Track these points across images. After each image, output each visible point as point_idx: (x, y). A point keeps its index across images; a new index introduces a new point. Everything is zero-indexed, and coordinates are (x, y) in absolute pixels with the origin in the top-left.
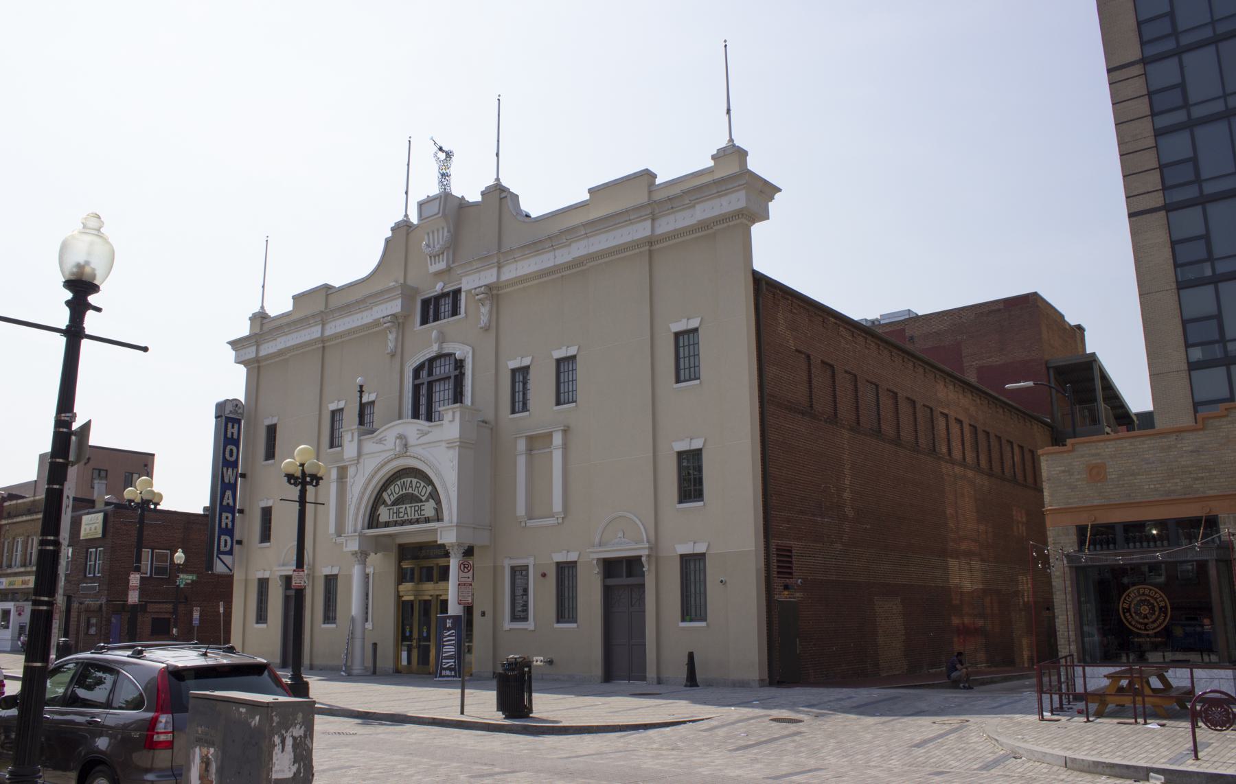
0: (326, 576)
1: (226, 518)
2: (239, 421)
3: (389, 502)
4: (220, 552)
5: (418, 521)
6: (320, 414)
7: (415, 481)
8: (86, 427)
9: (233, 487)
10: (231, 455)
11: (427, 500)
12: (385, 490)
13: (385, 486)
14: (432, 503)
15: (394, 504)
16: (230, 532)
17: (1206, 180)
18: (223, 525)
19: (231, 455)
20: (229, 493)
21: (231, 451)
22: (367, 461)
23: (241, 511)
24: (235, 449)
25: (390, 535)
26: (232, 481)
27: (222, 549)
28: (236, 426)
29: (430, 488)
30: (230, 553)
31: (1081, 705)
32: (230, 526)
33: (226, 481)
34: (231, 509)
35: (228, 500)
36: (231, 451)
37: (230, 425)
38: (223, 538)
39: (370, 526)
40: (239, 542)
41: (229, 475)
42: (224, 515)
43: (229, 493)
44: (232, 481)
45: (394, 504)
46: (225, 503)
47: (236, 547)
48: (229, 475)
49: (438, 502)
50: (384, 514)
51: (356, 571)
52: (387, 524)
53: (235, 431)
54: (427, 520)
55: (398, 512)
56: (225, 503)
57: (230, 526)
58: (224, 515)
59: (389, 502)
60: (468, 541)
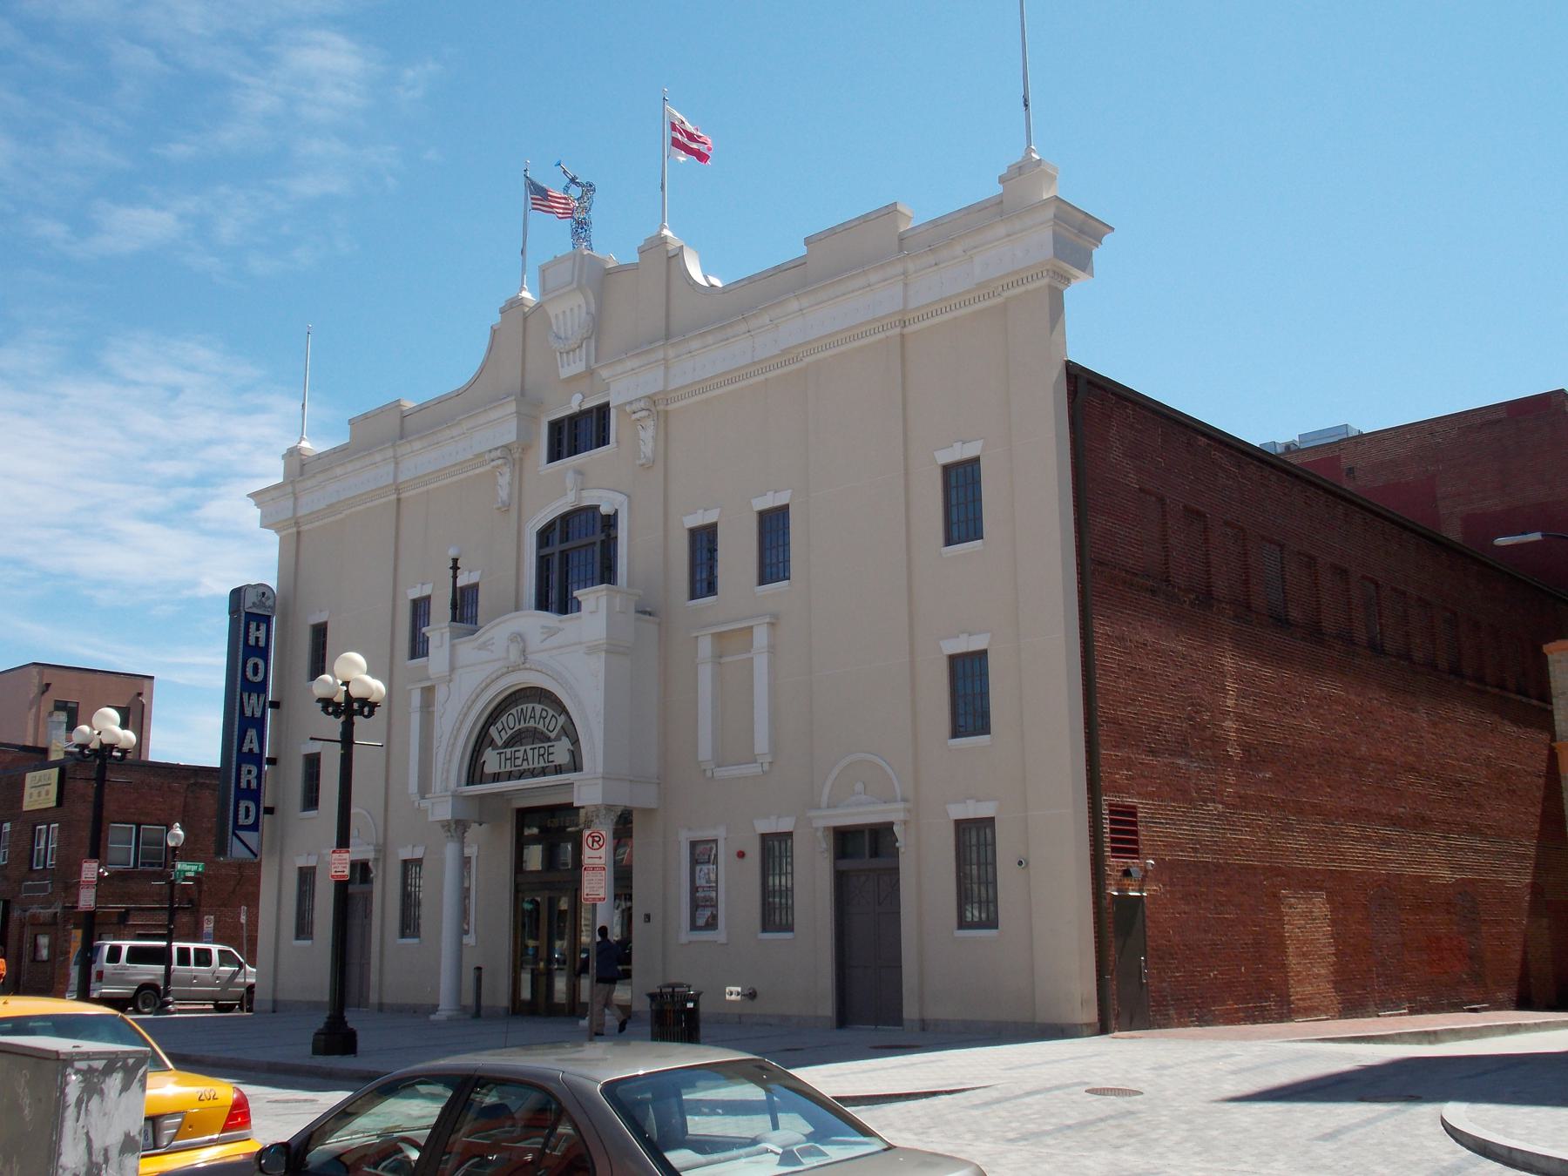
1: (248, 775)
3: (500, 743)
4: (237, 826)
7: (539, 707)
9: (259, 724)
10: (256, 672)
11: (558, 738)
15: (507, 744)
16: (254, 795)
18: (244, 785)
19: (256, 672)
20: (252, 733)
21: (256, 666)
22: (468, 672)
26: (258, 714)
27: (242, 821)
28: (263, 627)
29: (562, 719)
30: (255, 827)
32: (254, 785)
33: (248, 713)
34: (256, 759)
35: (251, 744)
36: (256, 666)
37: (253, 626)
38: (243, 804)
39: (471, 781)
40: (270, 811)
43: (252, 733)
44: (258, 714)
45: (507, 744)
46: (245, 749)
47: (266, 819)
48: (252, 705)
49: (575, 742)
50: (492, 761)
51: (450, 851)
52: (496, 777)
53: (262, 634)
54: (558, 770)
56: (245, 749)
57: (254, 785)
58: (245, 768)
60: (623, 800)
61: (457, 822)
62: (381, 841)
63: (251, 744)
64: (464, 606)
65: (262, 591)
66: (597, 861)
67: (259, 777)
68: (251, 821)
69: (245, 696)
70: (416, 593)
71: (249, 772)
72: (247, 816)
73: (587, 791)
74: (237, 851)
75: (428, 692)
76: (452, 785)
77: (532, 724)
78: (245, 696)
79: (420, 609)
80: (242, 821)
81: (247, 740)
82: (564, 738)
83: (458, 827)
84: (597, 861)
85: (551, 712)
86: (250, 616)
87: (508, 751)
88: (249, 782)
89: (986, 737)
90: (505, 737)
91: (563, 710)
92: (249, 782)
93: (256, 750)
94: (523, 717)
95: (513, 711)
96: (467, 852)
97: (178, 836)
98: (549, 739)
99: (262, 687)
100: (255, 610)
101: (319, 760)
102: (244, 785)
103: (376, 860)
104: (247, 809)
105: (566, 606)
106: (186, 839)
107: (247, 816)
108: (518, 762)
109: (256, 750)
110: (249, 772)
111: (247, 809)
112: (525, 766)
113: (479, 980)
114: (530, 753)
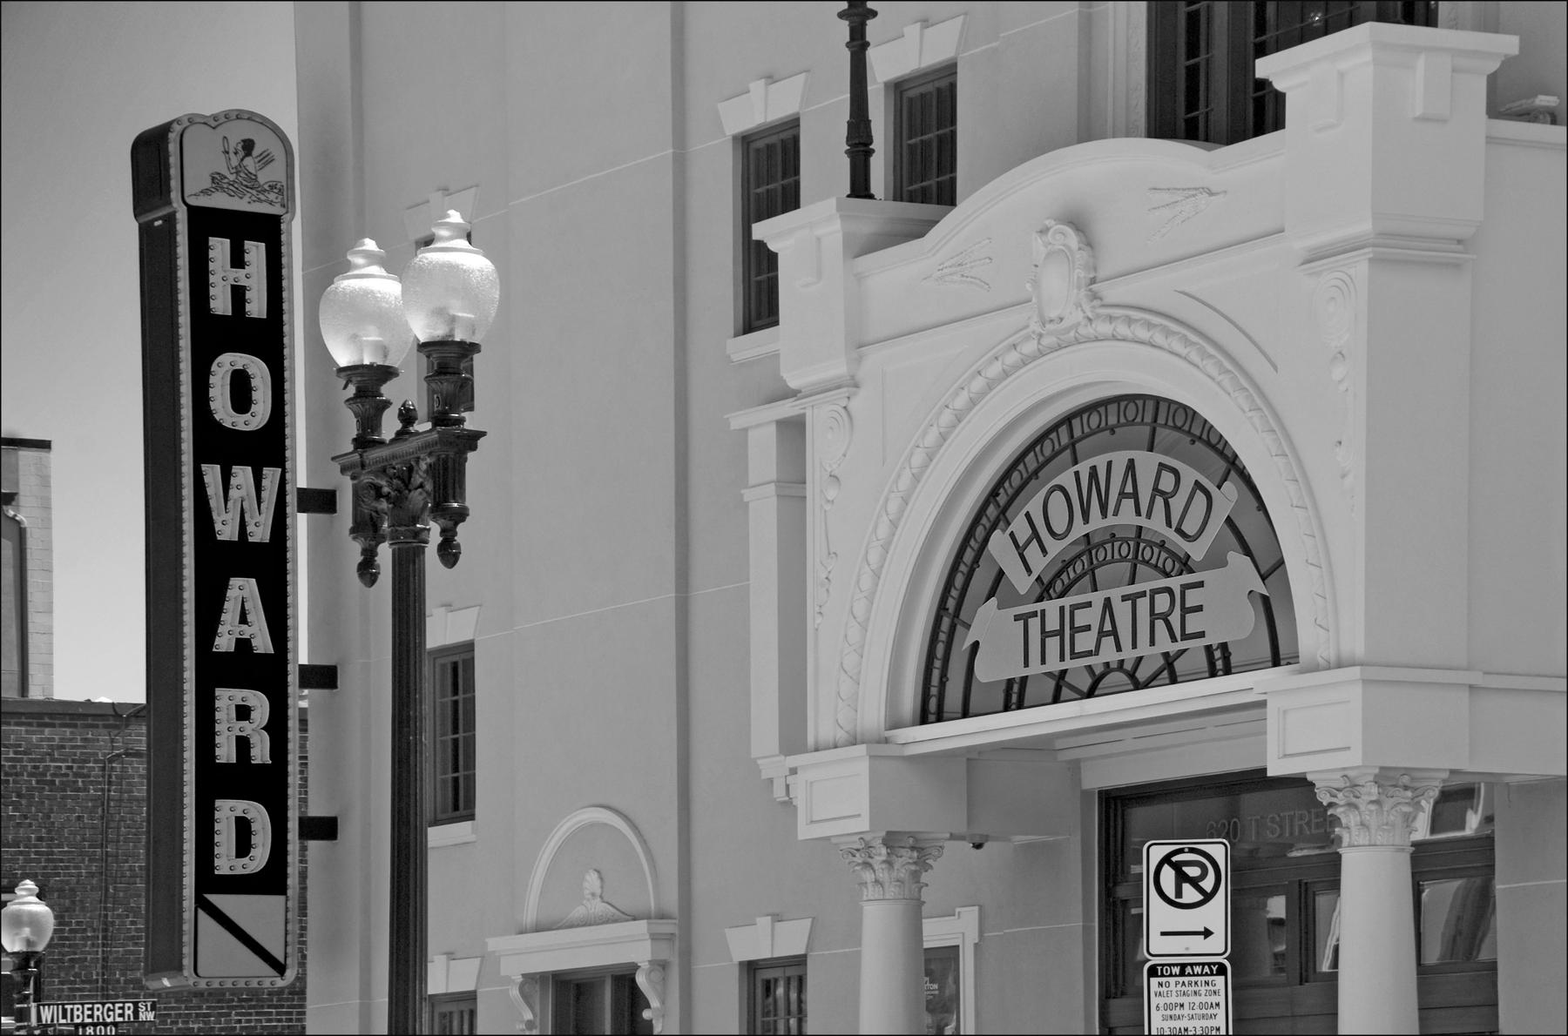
0: (751, 968)
1: (241, 718)
2: (268, 230)
3: (1022, 582)
4: (209, 881)
5: (1170, 671)
6: (680, 162)
7: (1147, 463)
8: (874, 14)
9: (269, 565)
11: (1216, 560)
12: (1002, 519)
13: (996, 506)
14: (1241, 572)
15: (1045, 590)
16: (266, 783)
17: (356, 24)
18: (226, 752)
20: (243, 590)
22: (922, 362)
23: (322, 677)
24: (258, 370)
25: (1040, 747)
26: (260, 532)
27: (226, 862)
28: (256, 252)
29: (1228, 497)
30: (271, 880)
31: (327, 599)
32: (261, 752)
33: (226, 530)
34: (265, 671)
35: (242, 617)
37: (219, 248)
39: (929, 712)
40: (323, 829)
41: (240, 503)
42: (227, 699)
43: (243, 590)
44: (260, 532)
45: (1045, 590)
46: (224, 642)
48: (240, 503)
49: (1273, 569)
50: (997, 641)
51: (878, 921)
52: (1014, 696)
54: (1220, 662)
55: (1069, 629)
56: (224, 642)
57: (261, 752)
58: (227, 699)
59: (1022, 582)
60: (1448, 753)
61: (892, 841)
62: (671, 902)
63: (242, 617)
64: (920, 155)
65: (249, 139)
66: (1197, 944)
67: (277, 727)
68: (259, 858)
69: (212, 473)
70: (758, 110)
71: (243, 713)
72: (243, 847)
73: (1307, 726)
74: (219, 959)
75: (793, 430)
76: (873, 715)
77: (1127, 516)
78: (212, 473)
79: (770, 170)
80: (226, 862)
81: (230, 616)
82: (1237, 559)
83: (907, 847)
84: (1197, 944)
85: (1189, 475)
86: (206, 222)
87: (1052, 607)
88: (243, 744)
89: (465, 826)
90: (1039, 563)
91: (1234, 467)
92: (243, 744)
93: (263, 644)
94: (1109, 514)
95: (1066, 479)
96: (936, 933)
97: (34, 921)
98: (1185, 565)
99: (267, 447)
100: (221, 201)
101: (470, 664)
102: (226, 752)
103: (662, 966)
104: (243, 828)
105: (1262, 112)
106: (60, 918)
107: (243, 847)
108: (1085, 642)
109: (263, 644)
110: (243, 713)
111: (243, 828)
112: (1108, 654)
113: (1158, 749)
114: (1122, 611)
